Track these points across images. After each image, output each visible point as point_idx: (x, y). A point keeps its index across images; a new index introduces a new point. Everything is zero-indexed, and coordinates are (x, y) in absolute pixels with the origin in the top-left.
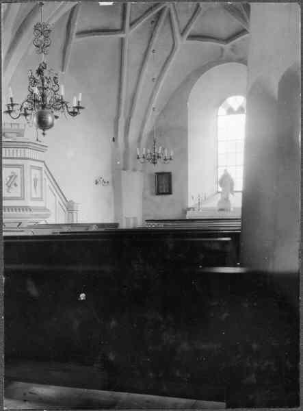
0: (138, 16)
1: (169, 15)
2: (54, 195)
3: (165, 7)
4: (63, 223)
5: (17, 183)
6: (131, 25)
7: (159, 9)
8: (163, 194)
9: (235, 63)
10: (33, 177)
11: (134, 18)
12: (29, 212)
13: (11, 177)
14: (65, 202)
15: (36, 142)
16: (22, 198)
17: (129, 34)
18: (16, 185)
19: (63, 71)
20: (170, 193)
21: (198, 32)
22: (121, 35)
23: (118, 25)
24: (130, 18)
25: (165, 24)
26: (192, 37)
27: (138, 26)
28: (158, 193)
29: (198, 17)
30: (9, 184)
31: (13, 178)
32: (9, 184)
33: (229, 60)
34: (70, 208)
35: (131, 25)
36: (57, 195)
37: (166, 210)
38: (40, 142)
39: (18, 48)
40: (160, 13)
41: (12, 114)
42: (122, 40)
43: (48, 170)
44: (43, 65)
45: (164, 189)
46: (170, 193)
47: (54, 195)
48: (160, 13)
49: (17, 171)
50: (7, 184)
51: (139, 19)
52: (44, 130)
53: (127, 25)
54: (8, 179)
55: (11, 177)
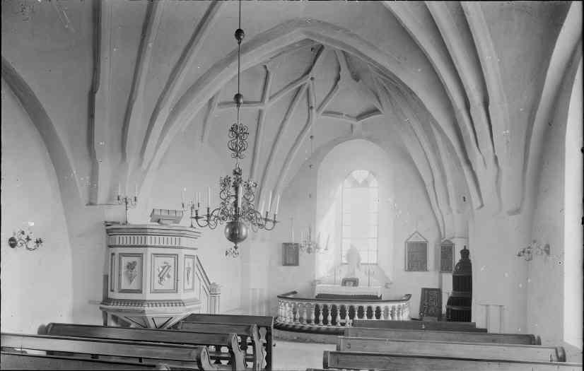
0: (277, 91)
1: (308, 90)
2: (200, 280)
3: (305, 84)
4: (205, 313)
5: (170, 274)
6: (270, 98)
7: (299, 85)
8: (289, 265)
9: (363, 140)
10: (186, 266)
11: (273, 93)
12: (182, 307)
13: (164, 268)
14: (208, 285)
15: (191, 229)
16: (140, 291)
17: (268, 106)
18: (169, 276)
19: (202, 142)
20: (296, 264)
21: (328, 110)
22: (260, 107)
23: (258, 99)
24: (270, 91)
25: (303, 99)
26: (326, 113)
27: (277, 99)
28: (285, 264)
29: (334, 95)
30: (161, 276)
31: (166, 268)
32: (161, 276)
33: (359, 136)
34: (212, 291)
35: (270, 98)
36: (202, 279)
37: (294, 280)
38: (195, 228)
39: (175, 123)
40: (299, 89)
41: (199, 220)
42: (260, 112)
43: (200, 263)
44: (237, 171)
45: (291, 260)
46: (296, 264)
47: (200, 280)
48: (299, 89)
49: (171, 261)
50: (159, 276)
51: (276, 94)
52: (236, 243)
53: (267, 100)
54: (161, 269)
55: (164, 268)
